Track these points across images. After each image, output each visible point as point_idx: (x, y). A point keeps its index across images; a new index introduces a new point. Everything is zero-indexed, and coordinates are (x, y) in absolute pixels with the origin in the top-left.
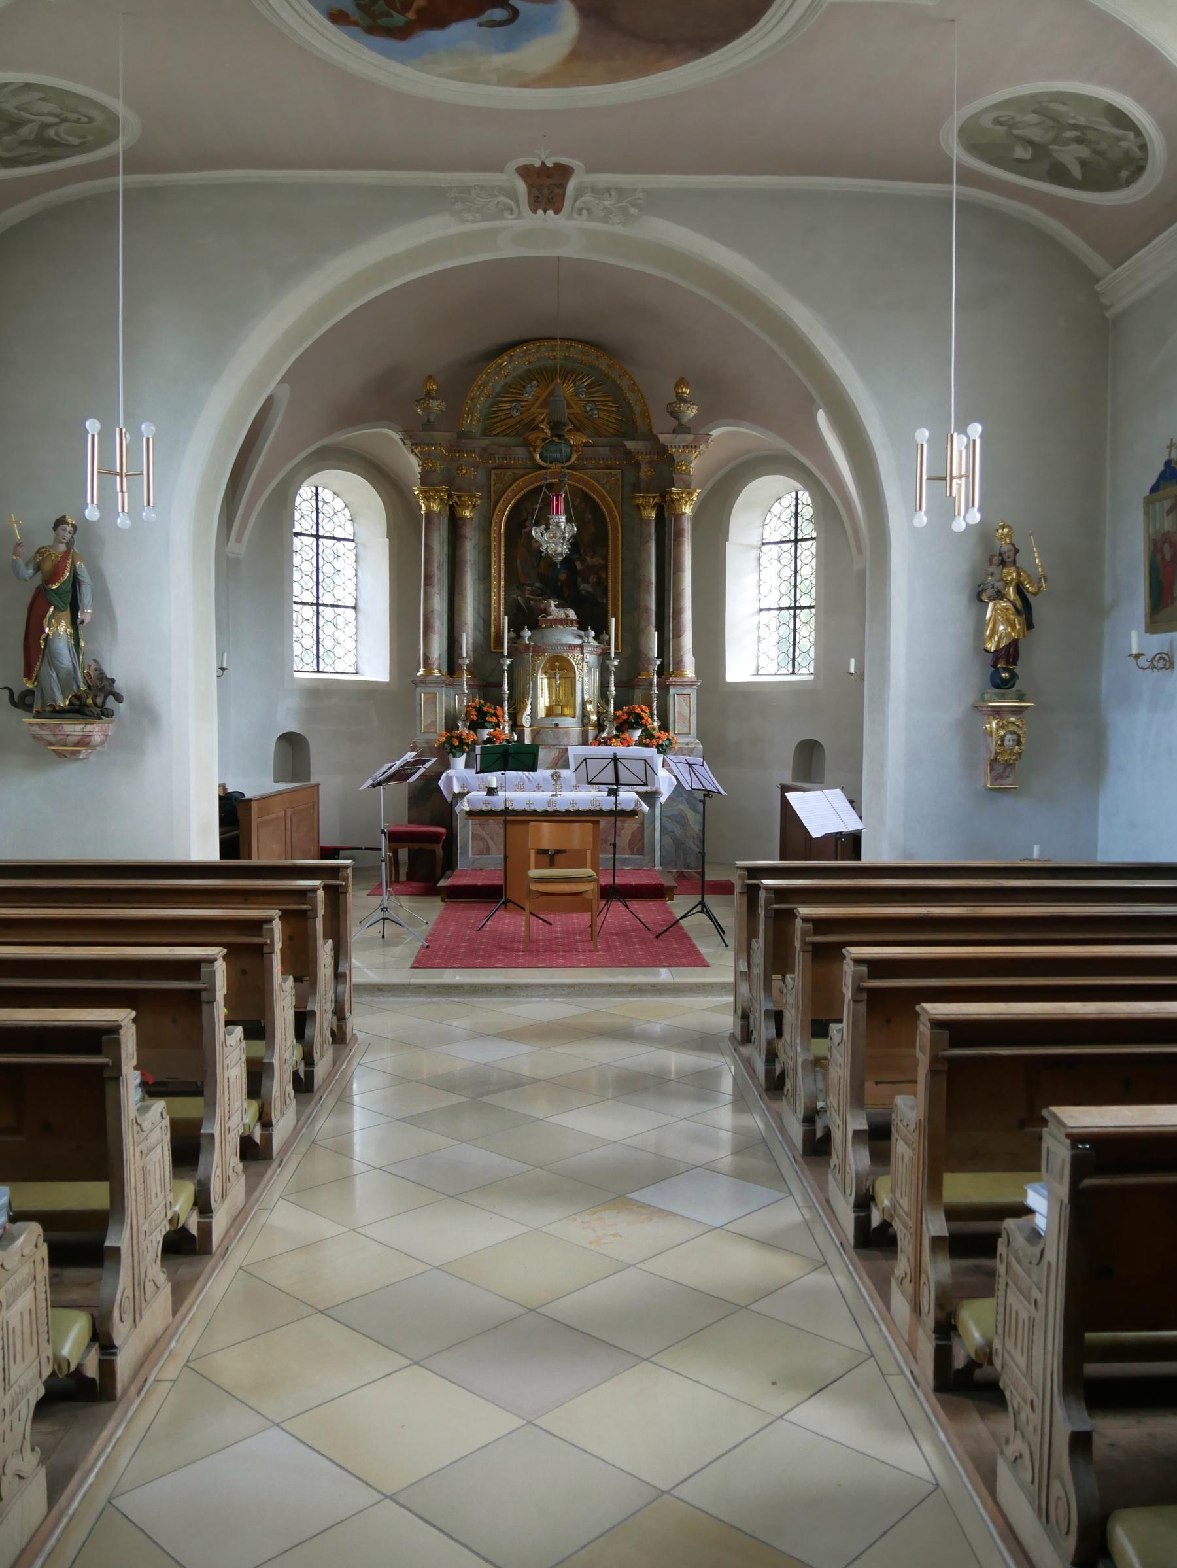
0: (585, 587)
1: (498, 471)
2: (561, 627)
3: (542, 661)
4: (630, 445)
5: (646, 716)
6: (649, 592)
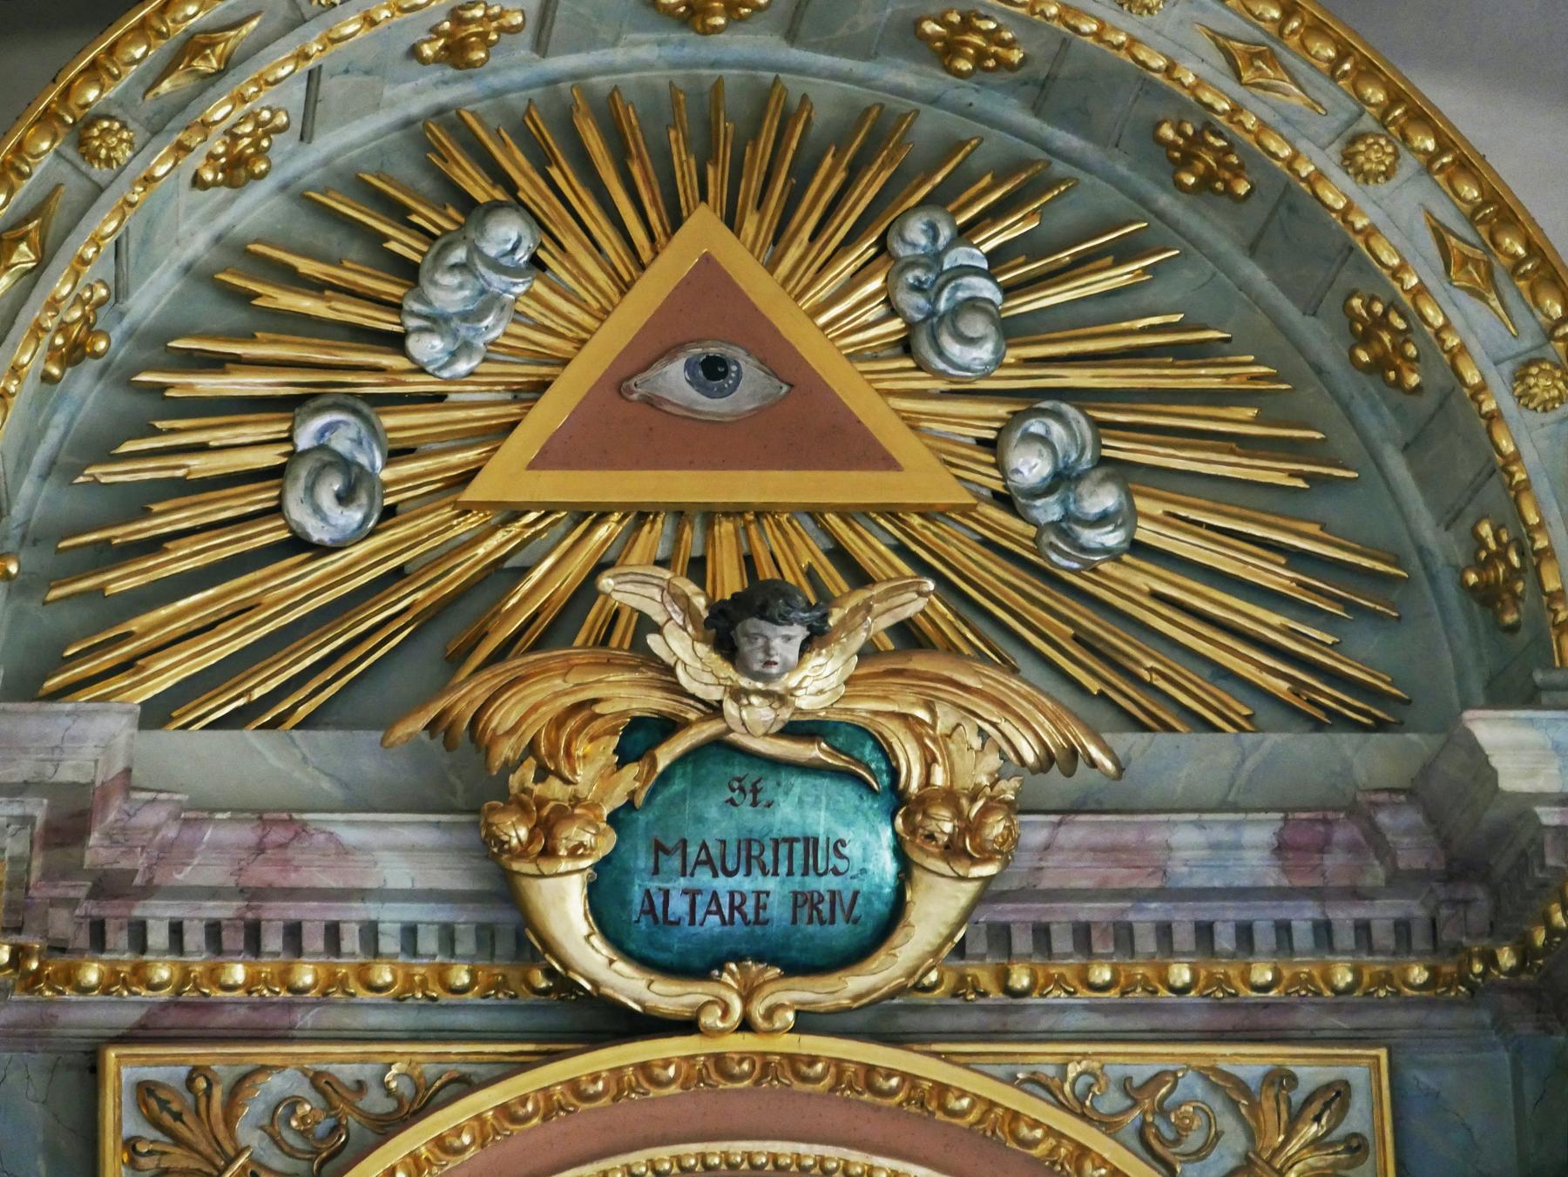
1: (165, 1066)
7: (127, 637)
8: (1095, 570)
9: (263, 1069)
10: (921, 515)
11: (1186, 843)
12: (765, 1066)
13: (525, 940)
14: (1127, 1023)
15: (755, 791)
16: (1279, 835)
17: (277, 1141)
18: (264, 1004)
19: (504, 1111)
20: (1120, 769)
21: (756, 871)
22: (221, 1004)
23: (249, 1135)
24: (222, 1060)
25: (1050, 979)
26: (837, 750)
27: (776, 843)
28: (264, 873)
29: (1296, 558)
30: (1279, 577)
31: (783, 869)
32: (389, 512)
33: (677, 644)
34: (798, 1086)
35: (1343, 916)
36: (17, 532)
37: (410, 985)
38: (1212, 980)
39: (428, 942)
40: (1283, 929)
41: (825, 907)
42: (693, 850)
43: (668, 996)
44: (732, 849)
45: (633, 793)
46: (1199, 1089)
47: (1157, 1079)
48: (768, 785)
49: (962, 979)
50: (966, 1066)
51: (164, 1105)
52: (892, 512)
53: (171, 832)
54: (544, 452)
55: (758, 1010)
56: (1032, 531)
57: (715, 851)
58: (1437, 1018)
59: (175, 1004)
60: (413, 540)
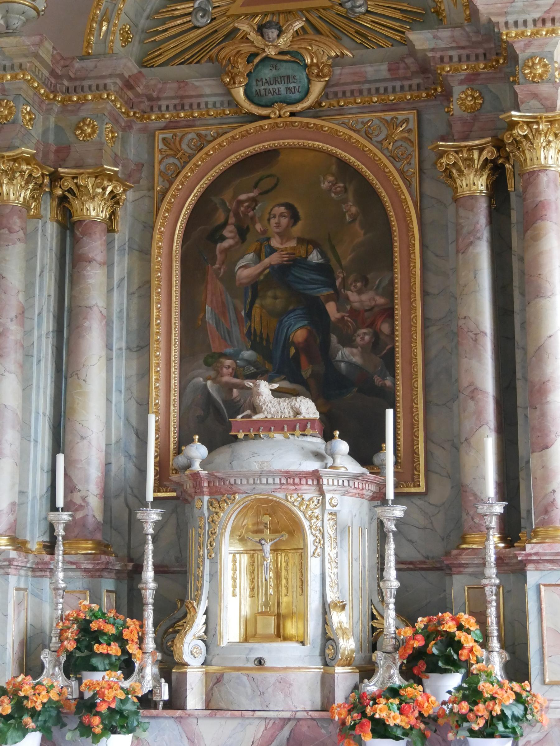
0: (347, 356)
1: (168, 135)
2: (278, 436)
3: (230, 516)
4: (421, 39)
5: (468, 641)
6: (480, 358)
7: (160, 49)
8: (359, 17)
9: (187, 133)
10: (323, 9)
11: (370, 71)
12: (286, 124)
13: (233, 103)
14: (366, 110)
15: (276, 67)
16: (388, 67)
17: (189, 147)
18: (188, 121)
19: (233, 137)
20: (353, 56)
21: (277, 83)
22: (179, 121)
23: (184, 146)
24: (179, 132)
25: (348, 102)
26: (292, 56)
27: (281, 77)
28: (181, 93)
29: (402, 11)
30: (398, 15)
31: (283, 82)
32: (215, 19)
33: (253, 36)
34: (293, 128)
35: (406, 83)
36: (140, 31)
37: (217, 114)
38: (382, 100)
39: (218, 105)
40: (394, 88)
41: (293, 90)
42: (264, 80)
43: (264, 112)
44: (272, 79)
45: (251, 70)
46: (378, 122)
47: (369, 121)
48: (278, 65)
49: (330, 104)
50: (329, 122)
51: (167, 142)
52: (317, 9)
53: (160, 86)
54: (243, 4)
55: (282, 113)
56: (346, 10)
57: (268, 80)
58: (430, 103)
59: (171, 122)
60: (219, 24)
